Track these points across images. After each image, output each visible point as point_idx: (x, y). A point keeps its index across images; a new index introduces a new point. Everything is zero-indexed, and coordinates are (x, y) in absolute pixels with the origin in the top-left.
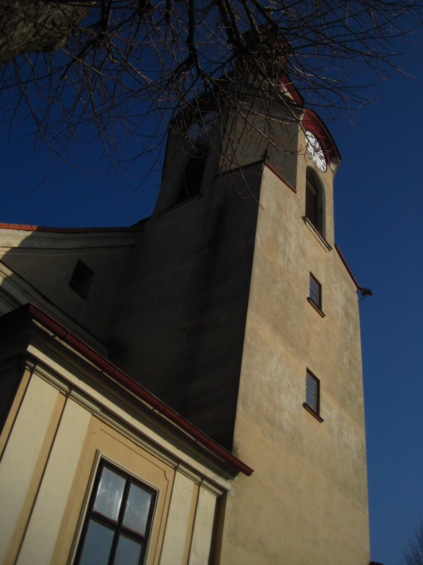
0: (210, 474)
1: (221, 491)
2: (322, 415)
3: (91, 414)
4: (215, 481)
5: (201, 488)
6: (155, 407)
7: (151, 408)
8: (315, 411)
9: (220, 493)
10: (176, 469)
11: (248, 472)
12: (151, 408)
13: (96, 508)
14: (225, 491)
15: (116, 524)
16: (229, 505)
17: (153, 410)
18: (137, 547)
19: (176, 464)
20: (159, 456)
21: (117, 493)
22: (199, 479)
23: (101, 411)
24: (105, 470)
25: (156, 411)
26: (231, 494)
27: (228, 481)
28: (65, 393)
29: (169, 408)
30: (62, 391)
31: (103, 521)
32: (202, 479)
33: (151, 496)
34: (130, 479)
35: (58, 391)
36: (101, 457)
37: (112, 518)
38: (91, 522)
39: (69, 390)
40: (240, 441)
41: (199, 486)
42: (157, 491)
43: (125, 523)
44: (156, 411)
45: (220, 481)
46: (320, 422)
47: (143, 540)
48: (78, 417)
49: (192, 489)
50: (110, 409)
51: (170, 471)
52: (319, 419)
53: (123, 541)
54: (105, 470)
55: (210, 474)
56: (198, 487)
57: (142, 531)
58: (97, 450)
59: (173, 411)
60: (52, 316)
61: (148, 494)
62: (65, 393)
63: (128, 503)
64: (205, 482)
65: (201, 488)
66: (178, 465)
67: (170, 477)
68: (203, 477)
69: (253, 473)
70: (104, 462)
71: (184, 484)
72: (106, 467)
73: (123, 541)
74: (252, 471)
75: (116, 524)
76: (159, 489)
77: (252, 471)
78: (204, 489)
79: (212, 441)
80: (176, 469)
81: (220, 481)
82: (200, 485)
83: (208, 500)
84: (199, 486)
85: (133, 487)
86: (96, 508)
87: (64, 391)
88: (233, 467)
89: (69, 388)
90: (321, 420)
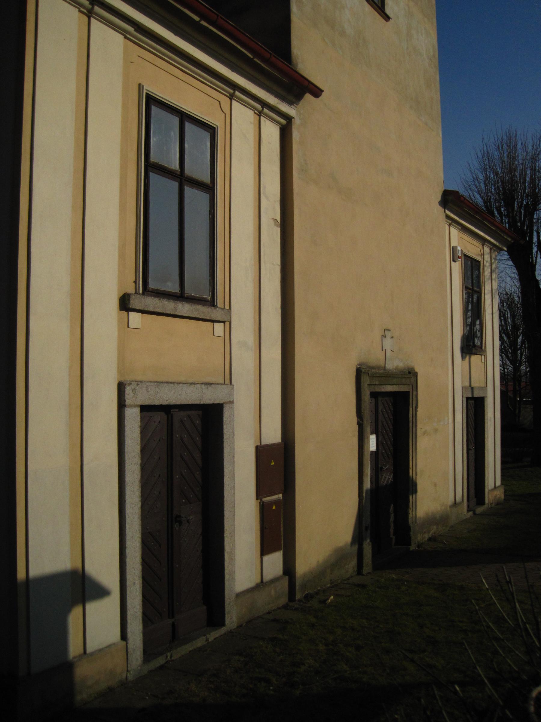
0: (272, 100)
1: (284, 120)
2: (388, 11)
3: (123, 37)
4: (278, 108)
5: (262, 118)
6: (203, 17)
7: (197, 19)
8: (380, 5)
9: (283, 122)
10: (231, 97)
11: (317, 92)
12: (197, 19)
13: (153, 158)
14: (289, 119)
15: (179, 173)
16: (296, 135)
17: (200, 21)
18: (203, 197)
19: (232, 91)
20: (211, 82)
21: (172, 134)
22: (259, 107)
23: (135, 30)
24: (154, 110)
25: (203, 23)
26: (297, 122)
27: (292, 106)
28: (85, 11)
29: (221, 18)
30: (82, 9)
31: (165, 172)
32: (263, 107)
33: (209, 134)
34: (184, 117)
35: (77, 10)
36: (146, 93)
37: (173, 167)
38: (152, 175)
39: (90, 6)
40: (299, 54)
41: (260, 116)
42: (214, 128)
43: (188, 171)
44: (203, 23)
45: (284, 107)
46: (387, 21)
47: (209, 188)
48: (108, 42)
49: (252, 121)
50: (146, 27)
51: (225, 101)
52: (384, 16)
53: (189, 192)
54: (154, 110)
55: (272, 100)
56: (258, 117)
57: (207, 179)
58: (139, 85)
59: (226, 21)
60: (139, 275)
61: (206, 132)
62: (85, 11)
63: (186, 146)
64: (265, 110)
65: (262, 119)
66: (234, 92)
67: (227, 110)
68: (264, 104)
69: (323, 93)
70: (151, 98)
71: (243, 116)
72: (154, 106)
73: (189, 192)
74: (322, 91)
75: (179, 173)
76: (217, 124)
77: (322, 91)
78: (266, 119)
79: (275, 57)
80: (231, 97)
81: (284, 107)
82: (260, 114)
83: (271, 132)
84: (260, 116)
85: (188, 126)
86: (153, 158)
87: (84, 7)
88: (297, 87)
89: (91, 3)
90: (387, 18)
